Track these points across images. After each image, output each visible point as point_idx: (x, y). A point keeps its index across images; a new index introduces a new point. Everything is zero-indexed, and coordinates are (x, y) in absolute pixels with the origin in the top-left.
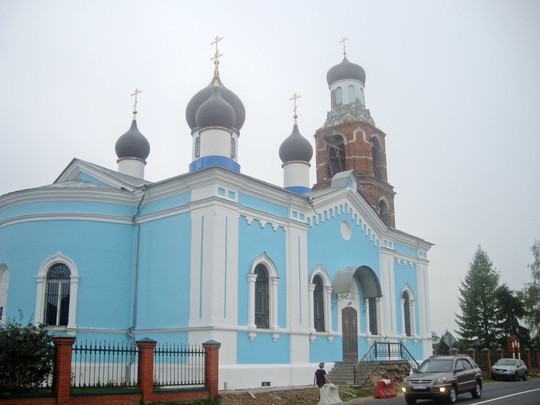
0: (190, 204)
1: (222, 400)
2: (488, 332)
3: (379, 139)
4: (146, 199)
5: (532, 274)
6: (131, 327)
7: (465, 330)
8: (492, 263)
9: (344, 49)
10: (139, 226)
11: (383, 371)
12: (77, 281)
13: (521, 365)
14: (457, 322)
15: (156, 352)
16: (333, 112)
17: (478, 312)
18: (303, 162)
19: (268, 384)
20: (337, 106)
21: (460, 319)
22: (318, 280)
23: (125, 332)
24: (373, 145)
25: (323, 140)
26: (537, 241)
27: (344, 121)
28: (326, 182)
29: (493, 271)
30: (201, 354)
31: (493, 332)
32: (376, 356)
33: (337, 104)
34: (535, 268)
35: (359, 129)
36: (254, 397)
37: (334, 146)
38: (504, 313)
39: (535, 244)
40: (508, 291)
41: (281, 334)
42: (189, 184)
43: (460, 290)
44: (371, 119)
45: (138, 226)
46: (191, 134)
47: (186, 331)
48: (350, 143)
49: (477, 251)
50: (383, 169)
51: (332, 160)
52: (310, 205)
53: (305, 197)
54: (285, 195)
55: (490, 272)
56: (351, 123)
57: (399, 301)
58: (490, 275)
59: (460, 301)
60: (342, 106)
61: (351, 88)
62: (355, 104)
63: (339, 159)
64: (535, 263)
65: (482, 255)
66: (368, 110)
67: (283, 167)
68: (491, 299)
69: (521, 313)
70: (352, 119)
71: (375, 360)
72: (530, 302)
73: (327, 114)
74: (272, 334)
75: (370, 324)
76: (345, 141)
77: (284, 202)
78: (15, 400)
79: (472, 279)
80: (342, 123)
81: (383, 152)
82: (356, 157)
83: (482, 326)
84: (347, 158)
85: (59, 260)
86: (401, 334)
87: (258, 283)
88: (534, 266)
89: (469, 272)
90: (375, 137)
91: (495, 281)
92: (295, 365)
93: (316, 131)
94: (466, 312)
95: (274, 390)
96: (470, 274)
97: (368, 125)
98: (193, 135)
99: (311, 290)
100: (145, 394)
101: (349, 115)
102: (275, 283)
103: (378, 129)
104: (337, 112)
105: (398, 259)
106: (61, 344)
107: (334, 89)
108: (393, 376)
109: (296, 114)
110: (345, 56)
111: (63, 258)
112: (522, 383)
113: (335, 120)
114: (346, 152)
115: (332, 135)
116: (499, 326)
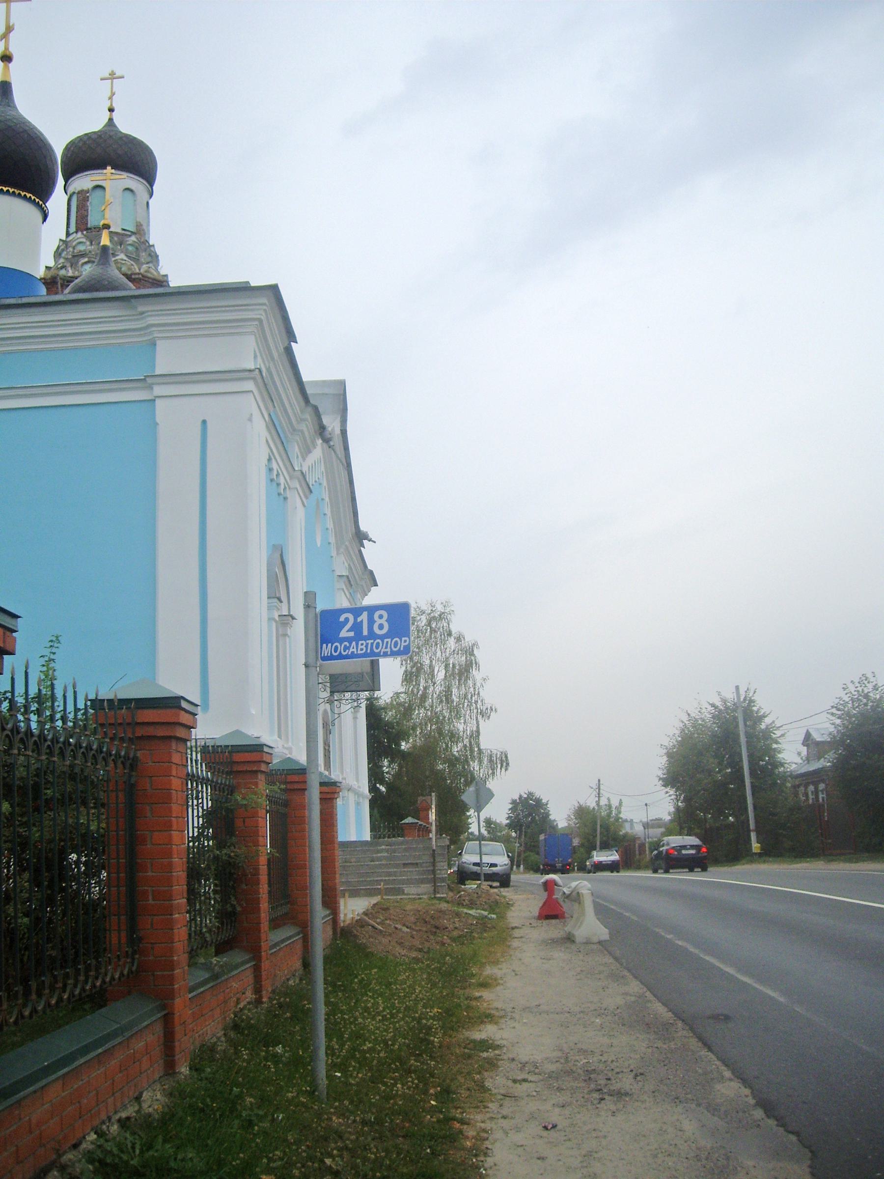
9: (111, 98)
16: (80, 243)
33: (89, 226)
61: (128, 193)
104: (91, 244)
107: (85, 188)
113: (86, 263)
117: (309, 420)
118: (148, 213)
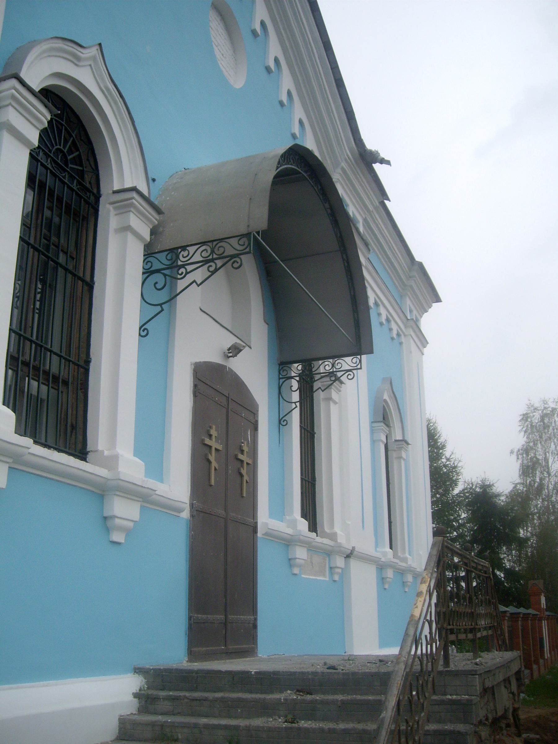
117: (417, 276)
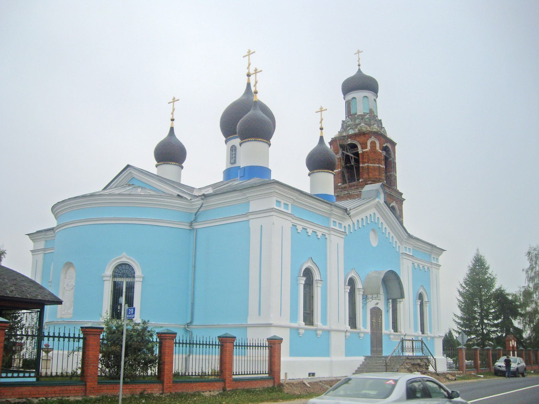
0: (249, 214)
1: (285, 388)
2: (484, 331)
3: (390, 148)
4: (203, 207)
5: (526, 278)
6: (189, 322)
7: (463, 329)
8: (489, 266)
9: (358, 61)
10: (196, 231)
11: (408, 365)
12: (141, 280)
13: (521, 363)
14: (455, 321)
15: (176, 343)
16: (348, 121)
17: (475, 312)
18: (329, 172)
19: (313, 374)
20: (351, 115)
21: (458, 319)
22: (351, 282)
23: (184, 326)
24: (385, 154)
25: (339, 146)
26: (532, 247)
27: (359, 130)
28: (341, 187)
29: (490, 274)
30: (217, 347)
31: (489, 331)
32: (403, 351)
33: (351, 114)
34: (529, 273)
35: (373, 139)
36: (309, 385)
37: (349, 154)
38: (500, 314)
39: (530, 250)
40: (505, 294)
41: (323, 330)
42: (248, 195)
43: (459, 291)
44: (384, 129)
45: (195, 231)
46: (225, 142)
47: (246, 327)
48: (364, 151)
49: (475, 255)
50: (394, 177)
51: (347, 167)
52: (348, 216)
53: (343, 208)
54: (327, 206)
55: (487, 275)
56: (366, 132)
57: (416, 302)
58: (486, 277)
59: (458, 301)
60: (356, 116)
61: (365, 98)
62: (369, 114)
63: (354, 167)
64: (530, 267)
65: (480, 258)
66: (381, 120)
67: (309, 175)
68: (488, 300)
69: (515, 314)
70: (366, 129)
71: (401, 355)
72: (524, 305)
73: (341, 123)
74: (316, 330)
75: (349, 318)
76: (359, 149)
77: (327, 213)
78: (134, 385)
79: (470, 280)
80: (357, 132)
81: (394, 160)
82: (370, 165)
83: (479, 326)
84: (361, 165)
85: (124, 260)
86: (417, 332)
87: (420, 305)
88: (529, 271)
89: (467, 274)
90: (387, 147)
91: (492, 284)
92: (334, 358)
93: (332, 138)
94: (464, 312)
95: (322, 380)
96: (468, 276)
97: (381, 135)
98: (227, 144)
99: (347, 292)
100: (227, 381)
101: (364, 125)
102: (319, 285)
103: (390, 139)
105: (415, 263)
106: (166, 339)
108: (415, 369)
109: (322, 126)
110: (359, 67)
111: (128, 259)
112: (521, 379)
113: (350, 129)
114: (360, 160)
115: (348, 143)
116: (496, 325)
118: (376, 104)
